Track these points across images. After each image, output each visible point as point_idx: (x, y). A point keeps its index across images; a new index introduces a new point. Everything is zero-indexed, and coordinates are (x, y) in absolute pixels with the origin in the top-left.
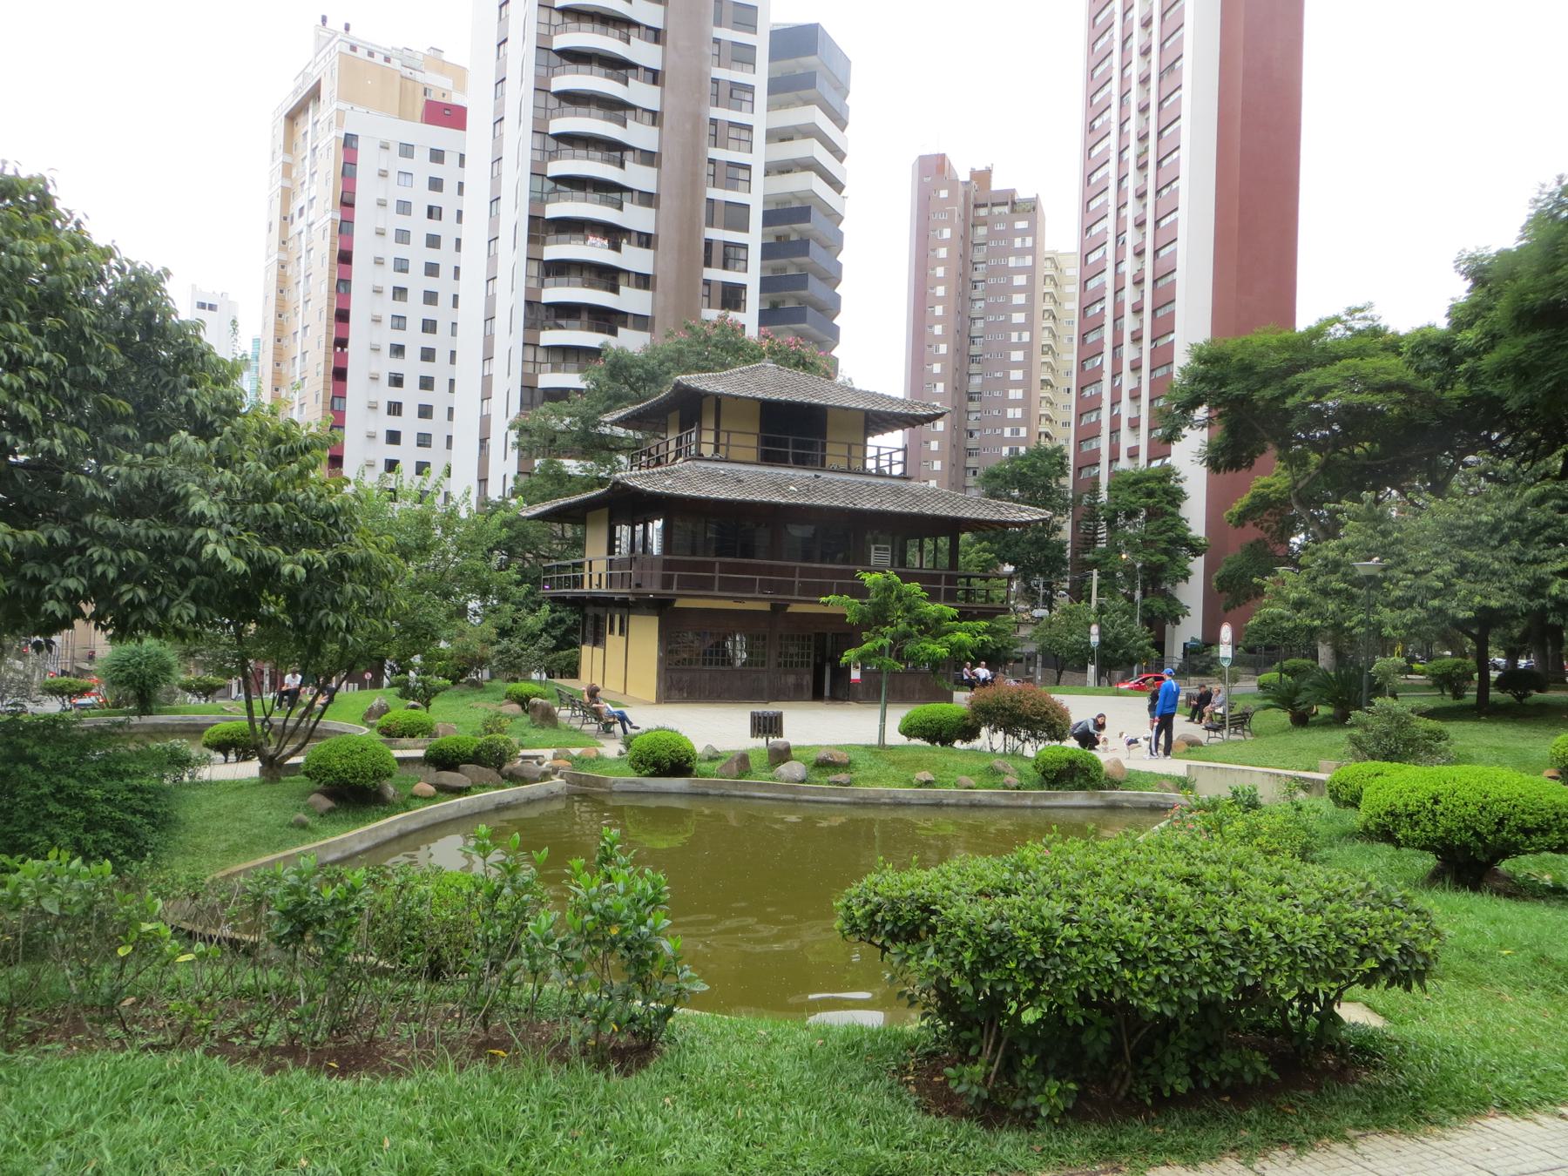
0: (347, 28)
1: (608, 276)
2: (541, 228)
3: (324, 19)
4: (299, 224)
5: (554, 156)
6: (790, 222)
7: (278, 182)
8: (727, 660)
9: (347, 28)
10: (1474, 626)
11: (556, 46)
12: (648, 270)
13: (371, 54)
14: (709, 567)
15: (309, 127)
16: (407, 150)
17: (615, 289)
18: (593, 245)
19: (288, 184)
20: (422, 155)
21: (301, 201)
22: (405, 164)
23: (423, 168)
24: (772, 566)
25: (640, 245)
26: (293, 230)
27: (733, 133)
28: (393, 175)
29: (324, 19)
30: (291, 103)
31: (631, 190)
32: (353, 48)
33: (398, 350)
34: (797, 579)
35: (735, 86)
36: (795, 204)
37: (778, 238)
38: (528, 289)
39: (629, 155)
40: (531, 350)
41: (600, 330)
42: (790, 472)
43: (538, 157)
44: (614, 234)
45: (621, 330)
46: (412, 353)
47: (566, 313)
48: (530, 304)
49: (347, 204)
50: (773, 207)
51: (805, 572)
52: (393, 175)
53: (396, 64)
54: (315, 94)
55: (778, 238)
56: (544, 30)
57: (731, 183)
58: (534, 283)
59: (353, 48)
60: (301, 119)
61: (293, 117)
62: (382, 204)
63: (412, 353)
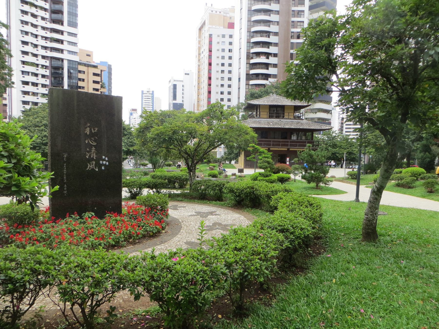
0: (212, 5)
1: (266, 66)
2: (249, 56)
3: (206, 4)
4: (202, 55)
5: (253, 37)
7: (198, 45)
9: (212, 5)
10: (403, 159)
11: (252, 9)
12: (276, 63)
13: (216, 12)
14: (270, 141)
15: (204, 31)
16: (224, 36)
17: (268, 69)
19: (200, 46)
20: (227, 37)
21: (202, 50)
22: (223, 40)
23: (227, 40)
25: (274, 57)
26: (201, 57)
27: (299, 24)
28: (220, 43)
29: (206, 4)
30: (200, 26)
32: (212, 11)
33: (222, 85)
35: (299, 11)
38: (247, 71)
39: (271, 34)
40: (247, 86)
41: (264, 79)
42: (274, 120)
43: (249, 38)
44: (267, 55)
45: (270, 47)
46: (226, 86)
47: (257, 76)
48: (248, 75)
49: (210, 51)
51: (273, 141)
52: (220, 43)
53: (222, 13)
54: (204, 23)
56: (250, 6)
58: (248, 69)
59: (212, 11)
60: (202, 30)
61: (200, 29)
62: (218, 50)
63: (226, 86)
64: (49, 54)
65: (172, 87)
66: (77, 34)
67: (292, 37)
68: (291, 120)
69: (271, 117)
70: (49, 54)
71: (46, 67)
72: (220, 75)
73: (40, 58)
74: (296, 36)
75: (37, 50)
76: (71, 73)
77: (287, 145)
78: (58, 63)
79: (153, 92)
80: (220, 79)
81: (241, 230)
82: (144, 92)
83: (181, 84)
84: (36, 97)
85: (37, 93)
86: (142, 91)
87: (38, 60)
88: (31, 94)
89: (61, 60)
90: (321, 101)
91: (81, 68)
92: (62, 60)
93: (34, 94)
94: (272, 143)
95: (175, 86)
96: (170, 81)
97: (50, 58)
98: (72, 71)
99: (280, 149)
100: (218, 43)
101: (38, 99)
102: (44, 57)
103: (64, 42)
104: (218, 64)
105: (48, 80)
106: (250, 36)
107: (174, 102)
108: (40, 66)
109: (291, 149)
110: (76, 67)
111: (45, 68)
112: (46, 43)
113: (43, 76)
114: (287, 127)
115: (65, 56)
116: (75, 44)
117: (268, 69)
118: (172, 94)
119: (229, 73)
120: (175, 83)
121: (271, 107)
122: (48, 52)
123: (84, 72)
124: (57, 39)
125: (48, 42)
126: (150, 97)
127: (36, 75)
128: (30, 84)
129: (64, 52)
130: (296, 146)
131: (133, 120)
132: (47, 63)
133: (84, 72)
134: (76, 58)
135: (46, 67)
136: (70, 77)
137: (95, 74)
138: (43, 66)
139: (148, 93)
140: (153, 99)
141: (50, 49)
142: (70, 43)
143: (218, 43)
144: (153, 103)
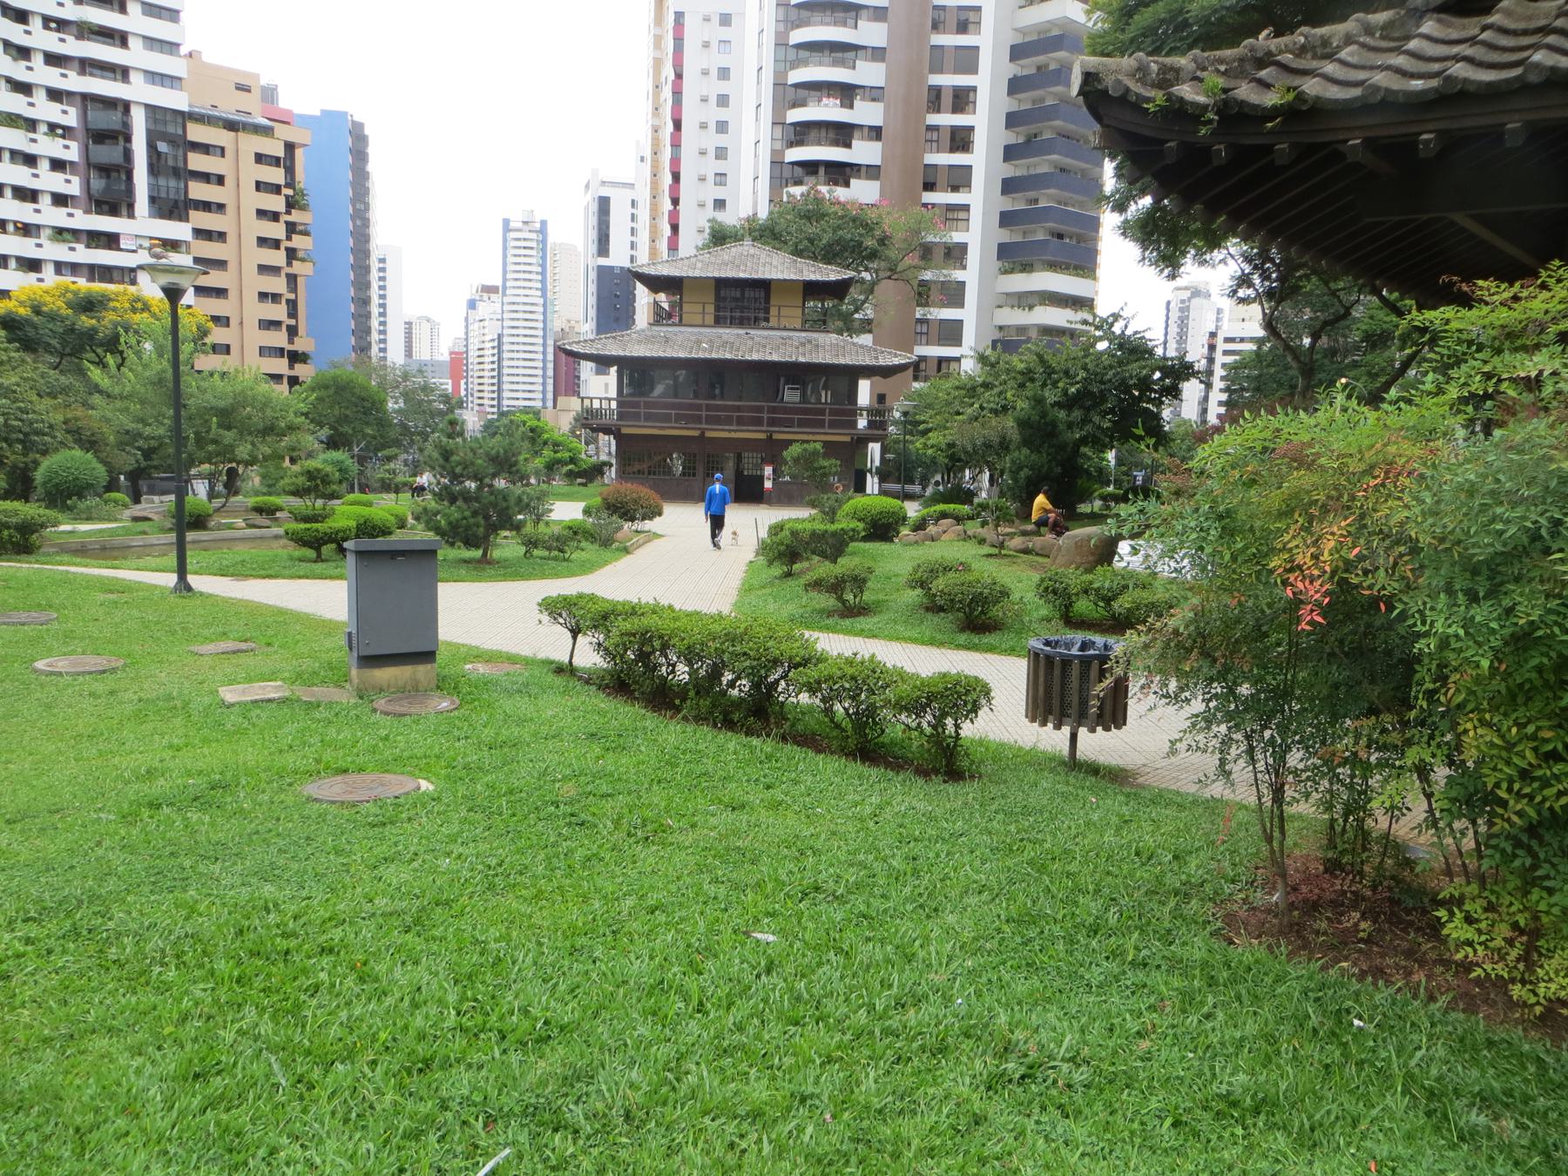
2: (790, 94)
6: (1045, 52)
8: (668, 470)
12: (878, 122)
17: (848, 145)
18: (826, 105)
24: (739, 407)
28: (714, 44)
31: (864, 48)
34: (642, 411)
36: (1055, 32)
37: (1039, 68)
39: (864, 13)
42: (727, 331)
43: (782, 27)
44: (846, 93)
45: (853, 182)
50: (1019, 40)
51: (708, 408)
52: (714, 44)
55: (1039, 68)
57: (963, 28)
58: (778, 145)
62: (705, 73)
64: (75, 82)
65: (594, 207)
66: (177, 12)
67: (936, 26)
68: (785, 334)
69: (719, 322)
70: (75, 82)
71: (67, 132)
72: (712, 166)
73: (40, 97)
74: (952, 22)
75: (30, 69)
76: (159, 154)
77: (698, 419)
78: (111, 120)
79: (544, 223)
80: (711, 178)
81: (685, 719)
82: (513, 225)
83: (629, 194)
84: (31, 241)
85: (38, 227)
86: (506, 222)
87: (31, 104)
88: (11, 228)
89: (120, 108)
90: (1054, 266)
91: (196, 133)
92: (126, 106)
93: (26, 230)
94: (704, 414)
95: (604, 205)
96: (587, 186)
97: (78, 99)
98: (163, 147)
99: (733, 435)
100: (706, 45)
101: (39, 246)
102: (55, 95)
103: (131, 41)
104: (704, 126)
105: (76, 180)
106: (786, 21)
107: (603, 261)
108: (43, 128)
109: (709, 434)
110: (180, 132)
111: (63, 137)
112: (62, 40)
113: (58, 165)
114: (755, 357)
115: (137, 91)
116: (170, 47)
117: (848, 145)
118: (593, 235)
119: (717, 158)
120: (604, 192)
121: (721, 283)
122: (72, 74)
123: (223, 149)
124: (100, 27)
125: (70, 39)
126: (534, 244)
127: (30, 160)
128: (13, 264)
129: (133, 76)
130: (728, 420)
131: (477, 325)
132: (71, 118)
133: (223, 149)
134: (176, 100)
135: (67, 132)
136: (154, 169)
137: (260, 158)
138: (52, 127)
139: (526, 228)
140: (544, 250)
141: (76, 64)
142: (152, 43)
143: (706, 45)
144: (543, 266)
